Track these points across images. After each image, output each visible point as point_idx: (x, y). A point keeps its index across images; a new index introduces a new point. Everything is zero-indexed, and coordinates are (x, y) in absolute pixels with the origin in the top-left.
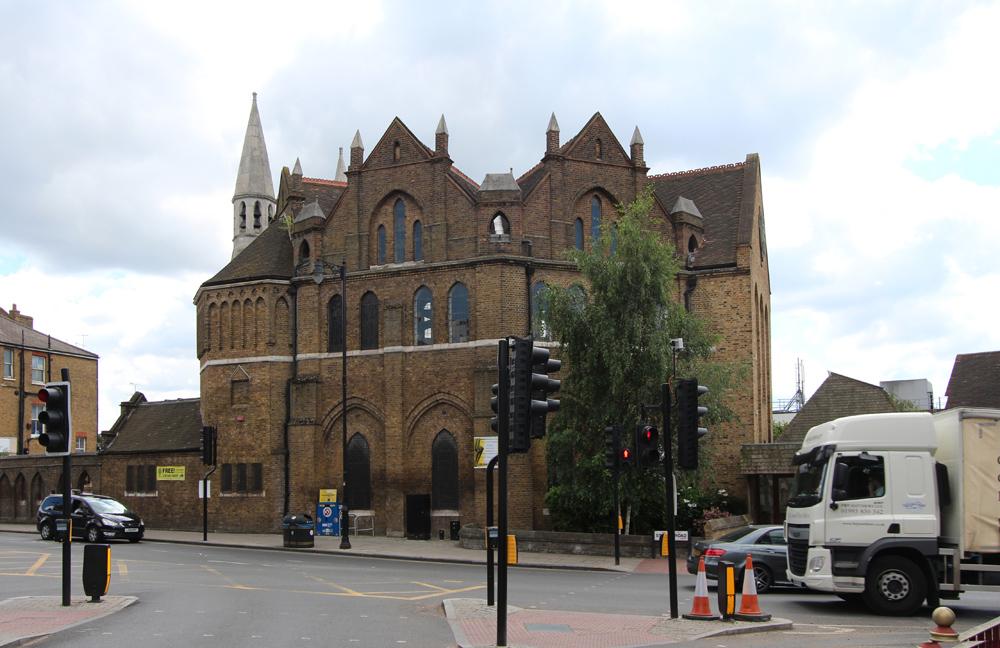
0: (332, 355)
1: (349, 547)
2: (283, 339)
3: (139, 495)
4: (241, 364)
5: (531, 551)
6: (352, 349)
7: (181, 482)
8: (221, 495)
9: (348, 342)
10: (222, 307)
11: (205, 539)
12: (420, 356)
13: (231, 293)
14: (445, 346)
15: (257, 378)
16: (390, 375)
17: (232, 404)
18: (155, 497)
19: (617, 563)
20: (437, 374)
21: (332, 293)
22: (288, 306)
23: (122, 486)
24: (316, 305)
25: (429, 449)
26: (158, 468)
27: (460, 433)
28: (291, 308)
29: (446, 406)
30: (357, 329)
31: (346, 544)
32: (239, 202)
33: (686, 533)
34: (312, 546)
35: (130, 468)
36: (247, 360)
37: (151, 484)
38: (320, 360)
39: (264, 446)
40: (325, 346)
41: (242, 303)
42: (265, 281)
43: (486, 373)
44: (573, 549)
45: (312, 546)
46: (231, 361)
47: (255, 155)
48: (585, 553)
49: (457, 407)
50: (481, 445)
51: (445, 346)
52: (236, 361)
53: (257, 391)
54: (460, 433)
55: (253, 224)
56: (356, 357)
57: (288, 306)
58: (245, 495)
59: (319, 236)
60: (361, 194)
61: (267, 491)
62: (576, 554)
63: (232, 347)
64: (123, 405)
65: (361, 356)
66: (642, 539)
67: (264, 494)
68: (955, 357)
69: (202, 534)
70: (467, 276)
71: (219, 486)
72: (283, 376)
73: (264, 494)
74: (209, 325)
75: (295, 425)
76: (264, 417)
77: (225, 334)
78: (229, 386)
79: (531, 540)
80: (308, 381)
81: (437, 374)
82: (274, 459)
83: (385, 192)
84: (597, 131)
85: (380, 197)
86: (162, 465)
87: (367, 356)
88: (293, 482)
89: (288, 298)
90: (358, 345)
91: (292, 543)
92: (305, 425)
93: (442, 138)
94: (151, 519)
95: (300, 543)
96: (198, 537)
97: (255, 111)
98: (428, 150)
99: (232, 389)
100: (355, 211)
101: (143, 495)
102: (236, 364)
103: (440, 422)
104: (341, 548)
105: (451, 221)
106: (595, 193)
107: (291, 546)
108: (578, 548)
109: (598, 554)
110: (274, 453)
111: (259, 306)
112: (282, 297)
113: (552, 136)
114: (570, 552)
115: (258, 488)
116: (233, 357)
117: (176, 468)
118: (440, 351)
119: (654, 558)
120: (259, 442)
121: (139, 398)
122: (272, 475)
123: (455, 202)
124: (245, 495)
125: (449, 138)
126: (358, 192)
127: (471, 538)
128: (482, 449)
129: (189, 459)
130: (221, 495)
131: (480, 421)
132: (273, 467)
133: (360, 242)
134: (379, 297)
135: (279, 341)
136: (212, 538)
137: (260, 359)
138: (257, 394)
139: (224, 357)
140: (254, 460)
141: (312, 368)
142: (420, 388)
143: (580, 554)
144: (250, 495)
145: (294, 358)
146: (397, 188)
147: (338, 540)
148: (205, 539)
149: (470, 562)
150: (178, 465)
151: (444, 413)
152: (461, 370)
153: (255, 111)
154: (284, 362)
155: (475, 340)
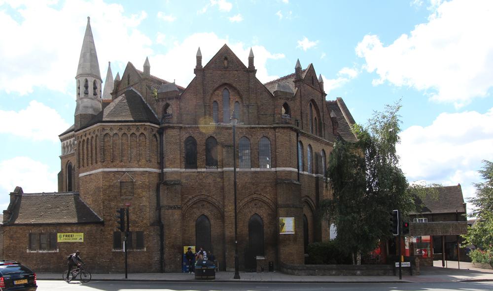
0: (188, 170)
1: (239, 278)
2: (155, 160)
3: (41, 252)
4: (128, 172)
5: (334, 275)
6: (201, 168)
7: (80, 243)
8: (113, 250)
9: (198, 164)
10: (113, 137)
11: (126, 277)
12: (243, 174)
13: (121, 129)
14: (258, 169)
15: (139, 181)
16: (228, 183)
17: (121, 195)
18: (57, 253)
19: (400, 279)
20: (253, 184)
21: (187, 135)
22: (157, 140)
23: (24, 246)
24: (178, 141)
25: (247, 224)
26: (58, 234)
27: (265, 215)
28: (159, 142)
29: (257, 201)
30: (205, 157)
31: (237, 276)
32: (83, 80)
33: (409, 263)
34: (214, 278)
35: (30, 235)
36: (132, 169)
37: (53, 244)
38: (181, 172)
39: (145, 221)
40: (183, 165)
41: (129, 135)
42: (146, 124)
43: (284, 185)
44: (356, 273)
45: (214, 278)
46: (120, 169)
47: (89, 54)
48: (362, 275)
49: (264, 202)
50: (284, 222)
51: (258, 169)
52: (124, 170)
53: (140, 188)
54: (265, 215)
55: (83, 91)
56: (204, 172)
57: (157, 140)
58: (131, 250)
59: (178, 102)
60: (204, 82)
61: (147, 248)
62: (358, 275)
63: (121, 161)
64: (11, 194)
65: (207, 172)
66: (388, 267)
67: (145, 249)
68: (15, 187)
69: (125, 275)
70: (270, 134)
71: (112, 246)
72: (155, 181)
73: (145, 249)
74: (104, 146)
75: (168, 209)
76: (145, 204)
77: (116, 153)
78: (118, 184)
79: (335, 269)
80: (175, 184)
81: (253, 184)
82: (152, 228)
83: (219, 83)
84: (225, 56)
85: (216, 86)
86: (62, 232)
87: (211, 172)
88: (166, 242)
89: (158, 135)
90: (184, 167)
91: (203, 277)
92: (175, 209)
93: (251, 60)
94: (51, 267)
95: (209, 277)
96: (122, 277)
97: (89, 28)
98: (246, 67)
99: (121, 186)
100: (201, 92)
101: (45, 252)
102: (124, 172)
103: (253, 210)
104: (234, 278)
105: (259, 104)
106: (226, 87)
107: (203, 279)
108: (359, 272)
109: (312, 275)
110: (152, 225)
111: (141, 138)
112: (124, 133)
113: (199, 59)
114: (355, 275)
115: (140, 245)
116: (122, 167)
117: (75, 234)
118: (256, 172)
119: (411, 275)
120: (141, 218)
121: (19, 191)
122: (151, 238)
123: (261, 94)
124: (131, 250)
125: (151, 68)
126: (203, 81)
127: (301, 270)
128: (284, 224)
129: (87, 228)
130: (113, 250)
131: (283, 209)
132: (152, 234)
133: (205, 108)
134: (218, 140)
135: (153, 160)
136: (131, 277)
137: (141, 169)
138: (140, 191)
139: (115, 167)
140: (137, 229)
141: (176, 177)
142: (244, 191)
143: (360, 275)
144: (135, 250)
145: (162, 171)
146: (227, 82)
147: (233, 275)
148: (126, 277)
149: (334, 282)
150: (77, 232)
151: (255, 205)
152: (267, 182)
153: (89, 28)
154: (155, 173)
155: (276, 167)
